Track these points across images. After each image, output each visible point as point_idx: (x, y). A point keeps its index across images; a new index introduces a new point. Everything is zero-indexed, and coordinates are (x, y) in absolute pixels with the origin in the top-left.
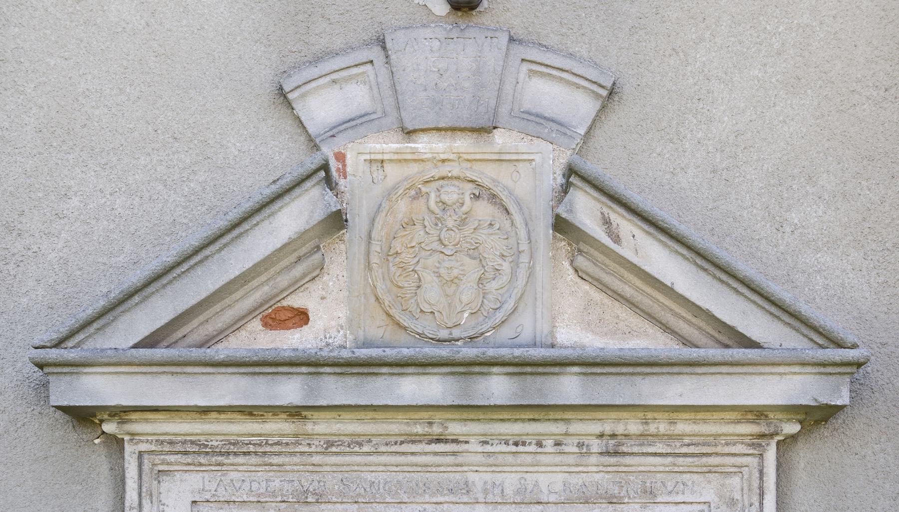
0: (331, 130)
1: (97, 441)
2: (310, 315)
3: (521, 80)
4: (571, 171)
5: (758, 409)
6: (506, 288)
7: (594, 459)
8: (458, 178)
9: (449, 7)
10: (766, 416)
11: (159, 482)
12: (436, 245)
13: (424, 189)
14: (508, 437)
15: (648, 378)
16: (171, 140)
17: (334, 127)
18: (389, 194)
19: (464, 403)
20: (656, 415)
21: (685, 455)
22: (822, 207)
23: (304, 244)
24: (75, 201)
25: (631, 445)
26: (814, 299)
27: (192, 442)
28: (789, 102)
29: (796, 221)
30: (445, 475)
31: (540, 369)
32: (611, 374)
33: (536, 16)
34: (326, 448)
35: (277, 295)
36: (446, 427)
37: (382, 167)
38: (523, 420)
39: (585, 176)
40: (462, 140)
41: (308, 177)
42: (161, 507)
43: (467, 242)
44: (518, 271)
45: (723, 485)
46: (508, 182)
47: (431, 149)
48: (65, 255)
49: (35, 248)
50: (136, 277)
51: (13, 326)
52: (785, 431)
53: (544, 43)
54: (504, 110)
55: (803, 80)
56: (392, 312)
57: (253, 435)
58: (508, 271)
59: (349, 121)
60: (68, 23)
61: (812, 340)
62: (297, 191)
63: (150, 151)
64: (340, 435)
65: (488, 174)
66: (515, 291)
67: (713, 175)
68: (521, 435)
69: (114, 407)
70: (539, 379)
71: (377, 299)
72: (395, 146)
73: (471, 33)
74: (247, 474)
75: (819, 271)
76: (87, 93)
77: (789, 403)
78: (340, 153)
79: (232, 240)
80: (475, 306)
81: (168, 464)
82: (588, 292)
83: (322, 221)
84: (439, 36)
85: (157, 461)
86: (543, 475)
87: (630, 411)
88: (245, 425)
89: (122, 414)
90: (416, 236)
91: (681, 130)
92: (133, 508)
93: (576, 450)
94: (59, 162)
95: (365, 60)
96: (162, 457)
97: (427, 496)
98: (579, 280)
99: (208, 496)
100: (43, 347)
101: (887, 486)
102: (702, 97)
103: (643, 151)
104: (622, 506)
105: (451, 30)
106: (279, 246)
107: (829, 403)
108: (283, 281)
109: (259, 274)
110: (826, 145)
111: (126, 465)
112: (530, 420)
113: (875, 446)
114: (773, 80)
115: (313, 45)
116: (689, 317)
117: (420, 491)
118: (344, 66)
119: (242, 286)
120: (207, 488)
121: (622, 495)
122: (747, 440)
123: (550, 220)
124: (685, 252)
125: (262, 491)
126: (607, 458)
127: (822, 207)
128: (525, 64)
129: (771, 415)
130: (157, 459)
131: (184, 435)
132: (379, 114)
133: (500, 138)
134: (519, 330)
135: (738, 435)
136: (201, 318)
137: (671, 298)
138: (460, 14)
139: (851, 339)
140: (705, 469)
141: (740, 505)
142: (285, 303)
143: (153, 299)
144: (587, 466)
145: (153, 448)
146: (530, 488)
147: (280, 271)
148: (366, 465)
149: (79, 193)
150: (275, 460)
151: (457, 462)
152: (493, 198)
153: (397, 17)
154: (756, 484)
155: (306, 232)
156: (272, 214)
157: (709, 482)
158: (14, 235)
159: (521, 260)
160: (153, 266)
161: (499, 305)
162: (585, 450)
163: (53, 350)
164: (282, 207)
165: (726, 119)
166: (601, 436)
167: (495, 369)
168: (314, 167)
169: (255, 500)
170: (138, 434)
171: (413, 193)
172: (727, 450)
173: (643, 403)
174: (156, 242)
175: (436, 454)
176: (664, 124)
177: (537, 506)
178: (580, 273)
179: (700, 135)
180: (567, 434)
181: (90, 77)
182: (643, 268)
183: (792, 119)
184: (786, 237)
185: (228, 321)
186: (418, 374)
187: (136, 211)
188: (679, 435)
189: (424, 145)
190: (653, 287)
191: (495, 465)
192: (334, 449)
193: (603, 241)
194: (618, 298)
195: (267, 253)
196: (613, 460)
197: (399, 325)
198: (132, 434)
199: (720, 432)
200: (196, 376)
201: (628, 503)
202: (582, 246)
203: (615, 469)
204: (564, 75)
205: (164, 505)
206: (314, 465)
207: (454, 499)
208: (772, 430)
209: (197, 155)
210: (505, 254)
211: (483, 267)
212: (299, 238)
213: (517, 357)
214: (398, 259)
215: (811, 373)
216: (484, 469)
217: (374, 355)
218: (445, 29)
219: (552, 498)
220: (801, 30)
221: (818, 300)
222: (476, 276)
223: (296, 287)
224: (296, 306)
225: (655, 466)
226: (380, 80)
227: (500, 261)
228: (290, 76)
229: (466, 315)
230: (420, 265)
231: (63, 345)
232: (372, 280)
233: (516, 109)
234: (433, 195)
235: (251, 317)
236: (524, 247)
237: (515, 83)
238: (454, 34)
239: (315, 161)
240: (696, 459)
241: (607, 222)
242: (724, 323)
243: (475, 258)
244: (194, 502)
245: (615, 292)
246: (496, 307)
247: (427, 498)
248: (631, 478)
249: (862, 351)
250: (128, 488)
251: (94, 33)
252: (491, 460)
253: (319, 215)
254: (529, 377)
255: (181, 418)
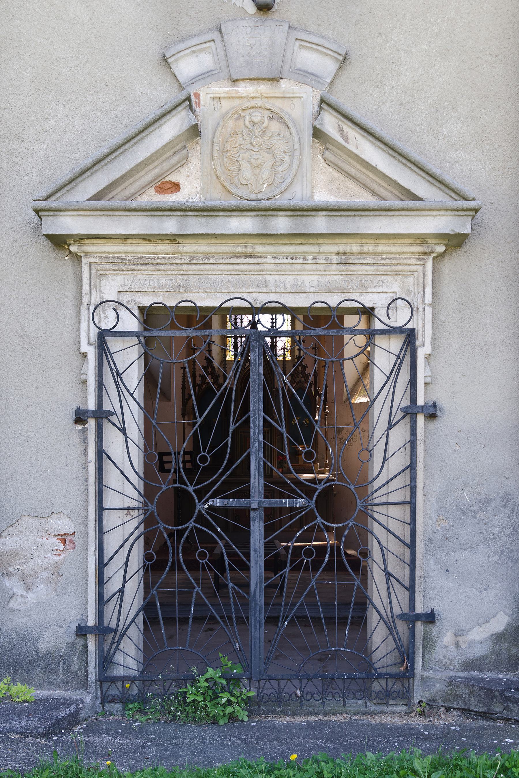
0: (192, 80)
1: (66, 258)
2: (181, 186)
3: (295, 51)
4: (322, 101)
5: (422, 237)
6: (286, 171)
7: (334, 267)
8: (261, 107)
9: (256, 8)
10: (427, 242)
11: (100, 280)
12: (249, 146)
13: (242, 114)
14: (288, 255)
15: (363, 218)
16: (104, 87)
17: (193, 78)
18: (223, 117)
19: (264, 232)
20: (367, 241)
21: (383, 265)
22: (460, 124)
23: (178, 145)
24: (53, 122)
25: (354, 259)
26: (455, 178)
27: (118, 257)
28: (442, 64)
29: (445, 133)
30: (254, 277)
31: (305, 213)
32: (343, 216)
33: (304, 14)
34: (190, 261)
35: (163, 174)
36: (254, 248)
37: (220, 101)
38: (296, 244)
39: (330, 103)
40: (263, 85)
41: (180, 104)
42: (102, 294)
43: (266, 144)
44: (294, 161)
45: (404, 282)
46: (289, 111)
47: (246, 90)
48: (48, 153)
49: (31, 149)
50: (88, 162)
51: (20, 193)
52: (437, 251)
53: (308, 30)
54: (286, 68)
55: (450, 51)
56: (225, 184)
57: (151, 253)
58: (288, 161)
59: (201, 75)
60: (47, 18)
61: (451, 196)
62: (174, 112)
63: (93, 93)
64: (197, 253)
65: (277, 105)
66: (292, 172)
67: (400, 106)
68: (294, 253)
69: (77, 235)
70: (304, 219)
71: (217, 177)
72: (226, 89)
73: (268, 23)
74: (147, 276)
75: (457, 162)
76: (58, 59)
77: (439, 232)
78: (197, 93)
79: (139, 140)
80: (270, 181)
81: (105, 270)
82: (331, 173)
83: (187, 130)
84: (250, 25)
85: (99, 268)
86: (307, 276)
87: (353, 239)
88: (146, 247)
89: (80, 240)
90: (238, 141)
91: (383, 80)
92: (87, 294)
93: (324, 262)
94: (44, 99)
95: (210, 39)
96: (102, 266)
97: (244, 289)
98: (326, 166)
99: (126, 288)
100: (39, 200)
101: (493, 283)
102: (395, 61)
103: (362, 93)
104: (349, 294)
105: (257, 21)
106: (164, 144)
107: (460, 232)
108: (166, 166)
109: (153, 162)
110: (463, 89)
111: (83, 270)
112: (299, 244)
113: (487, 261)
114: (434, 51)
115: (181, 31)
116: (386, 185)
117: (241, 286)
118: (198, 43)
119: (144, 168)
120: (126, 284)
121: (349, 288)
122: (417, 256)
123: (311, 131)
124: (383, 146)
125: (156, 285)
126: (341, 266)
127: (460, 124)
128: (297, 41)
129: (429, 241)
130: (99, 267)
131: (114, 253)
132: (218, 71)
133: (284, 84)
134: (294, 194)
135: (412, 253)
136: (122, 186)
137: (376, 175)
138: (262, 13)
139: (471, 195)
140: (394, 273)
141: (412, 294)
142: (167, 179)
143: (97, 174)
144: (330, 271)
145: (97, 260)
146: (299, 284)
147: (165, 160)
148: (211, 270)
149: (55, 117)
150: (163, 267)
151: (260, 269)
152: (280, 119)
153: (227, 15)
154: (421, 281)
155: (179, 136)
156: (160, 126)
157: (396, 281)
158: (20, 141)
159: (295, 155)
160: (97, 154)
161: (283, 180)
162: (329, 262)
163: (44, 202)
164: (165, 122)
165: (408, 74)
166: (338, 253)
167: (281, 213)
168: (183, 98)
169: (152, 290)
170: (89, 253)
171: (236, 116)
172: (406, 262)
173: (359, 232)
174: (97, 145)
175: (249, 264)
176: (374, 77)
177: (303, 294)
178: (327, 162)
179: (393, 83)
180: (319, 253)
181: (59, 50)
182: (361, 156)
183: (444, 74)
184: (440, 142)
185: (137, 188)
186: (239, 216)
187: (86, 127)
188: (380, 253)
189: (243, 88)
190: (366, 168)
191: (281, 271)
192: (194, 261)
193: (339, 141)
194: (348, 176)
195: (158, 148)
196: (344, 267)
197: (229, 191)
198: (86, 253)
199: (402, 251)
200: (120, 217)
201: (352, 292)
202: (328, 145)
203: (345, 273)
204: (319, 48)
205: (103, 293)
206: (183, 271)
207: (259, 290)
208: (430, 250)
209: (119, 95)
210: (286, 151)
211: (275, 158)
212: (175, 139)
213: (292, 206)
214: (228, 154)
215: (451, 215)
216: (275, 273)
217: (215, 205)
218: (254, 21)
219: (312, 290)
220: (450, 22)
221: (457, 178)
222: (271, 163)
223: (173, 170)
224: (173, 181)
225: (367, 271)
226: (218, 50)
227: (284, 155)
228: (169, 48)
229: (265, 186)
230: (240, 157)
231: (49, 200)
232: (214, 166)
233: (293, 68)
234: (247, 117)
235: (149, 187)
236: (297, 147)
237: (292, 52)
238: (259, 24)
239: (182, 96)
240: (389, 267)
241: (341, 130)
242: (404, 188)
243: (270, 154)
244: (119, 292)
245: (346, 172)
246: (281, 181)
247: (244, 290)
248: (354, 278)
249: (478, 202)
250: (84, 283)
251: (61, 24)
252: (279, 268)
253: (186, 126)
254: (298, 218)
255: (112, 243)
